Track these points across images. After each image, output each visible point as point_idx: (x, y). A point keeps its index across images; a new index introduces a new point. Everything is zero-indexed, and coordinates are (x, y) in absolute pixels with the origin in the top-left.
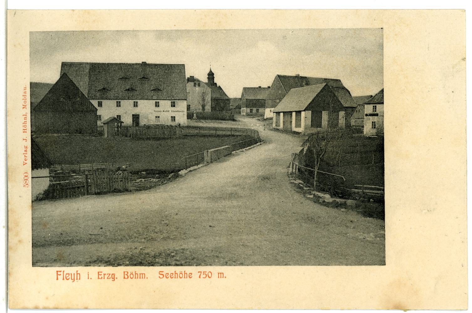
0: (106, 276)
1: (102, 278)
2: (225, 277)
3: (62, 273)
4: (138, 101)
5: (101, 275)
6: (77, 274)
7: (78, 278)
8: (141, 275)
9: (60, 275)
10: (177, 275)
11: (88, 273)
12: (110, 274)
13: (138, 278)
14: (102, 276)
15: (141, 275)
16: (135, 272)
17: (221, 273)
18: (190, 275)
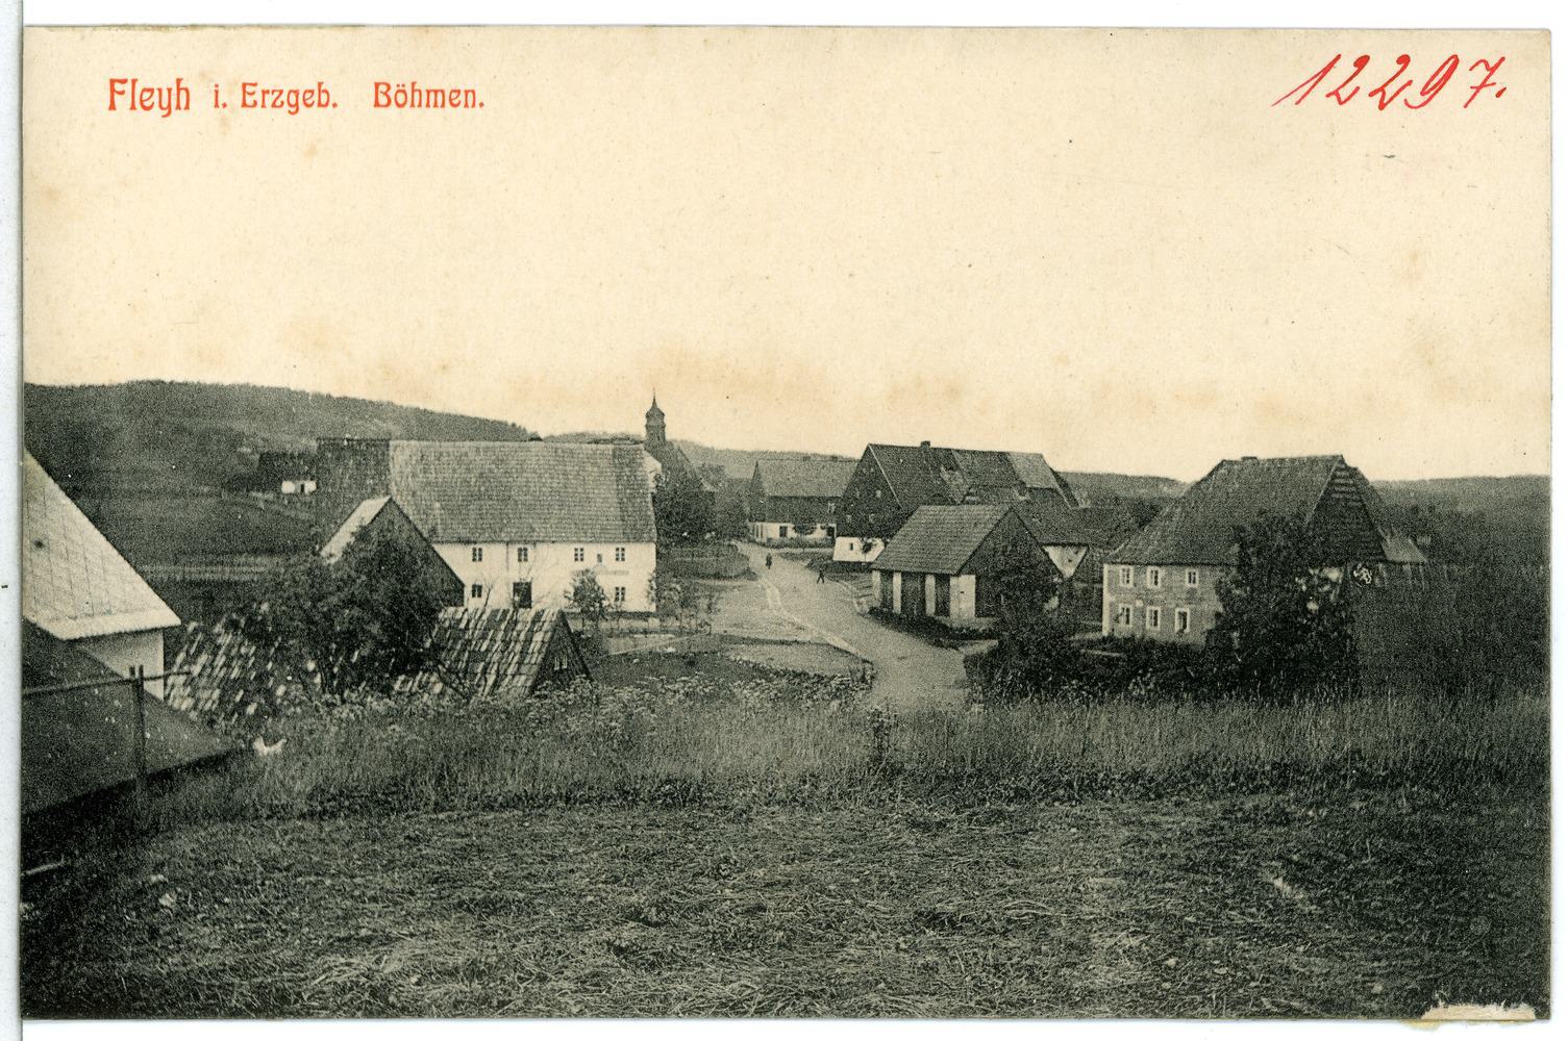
0: (270, 99)
1: (255, 103)
2: (335, 105)
3: (128, 87)
4: (484, 547)
5: (252, 94)
6: (179, 89)
7: (183, 103)
8: (432, 95)
9: (122, 93)
10: (420, 95)
11: (217, 86)
12: (281, 92)
13: (420, 105)
14: (258, 97)
15: (432, 95)
16: (413, 84)
17: (436, 92)
18: (454, 95)
